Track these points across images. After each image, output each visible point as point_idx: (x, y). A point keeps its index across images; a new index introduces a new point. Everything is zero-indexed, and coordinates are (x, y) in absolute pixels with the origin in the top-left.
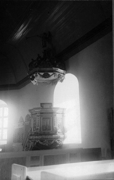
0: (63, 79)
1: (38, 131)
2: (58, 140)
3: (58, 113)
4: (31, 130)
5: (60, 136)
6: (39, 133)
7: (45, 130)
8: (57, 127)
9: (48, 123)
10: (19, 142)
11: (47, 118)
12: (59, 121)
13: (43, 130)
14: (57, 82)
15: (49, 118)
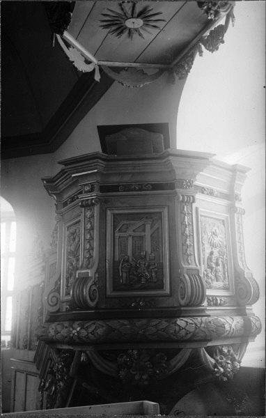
0: (222, 30)
1: (86, 292)
2: (211, 351)
3: (202, 190)
4: (58, 290)
5: (223, 326)
6: (92, 304)
7: (129, 287)
8: (203, 269)
9: (148, 246)
10: (28, 346)
11: (127, 188)
12: (214, 234)
13: (115, 289)
14: (192, 57)
15: (155, 217)
